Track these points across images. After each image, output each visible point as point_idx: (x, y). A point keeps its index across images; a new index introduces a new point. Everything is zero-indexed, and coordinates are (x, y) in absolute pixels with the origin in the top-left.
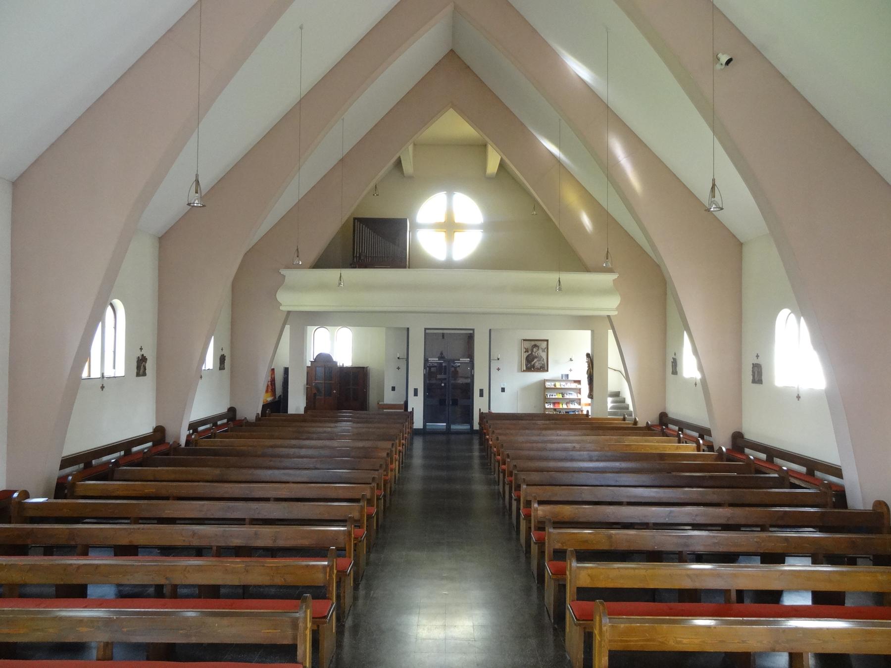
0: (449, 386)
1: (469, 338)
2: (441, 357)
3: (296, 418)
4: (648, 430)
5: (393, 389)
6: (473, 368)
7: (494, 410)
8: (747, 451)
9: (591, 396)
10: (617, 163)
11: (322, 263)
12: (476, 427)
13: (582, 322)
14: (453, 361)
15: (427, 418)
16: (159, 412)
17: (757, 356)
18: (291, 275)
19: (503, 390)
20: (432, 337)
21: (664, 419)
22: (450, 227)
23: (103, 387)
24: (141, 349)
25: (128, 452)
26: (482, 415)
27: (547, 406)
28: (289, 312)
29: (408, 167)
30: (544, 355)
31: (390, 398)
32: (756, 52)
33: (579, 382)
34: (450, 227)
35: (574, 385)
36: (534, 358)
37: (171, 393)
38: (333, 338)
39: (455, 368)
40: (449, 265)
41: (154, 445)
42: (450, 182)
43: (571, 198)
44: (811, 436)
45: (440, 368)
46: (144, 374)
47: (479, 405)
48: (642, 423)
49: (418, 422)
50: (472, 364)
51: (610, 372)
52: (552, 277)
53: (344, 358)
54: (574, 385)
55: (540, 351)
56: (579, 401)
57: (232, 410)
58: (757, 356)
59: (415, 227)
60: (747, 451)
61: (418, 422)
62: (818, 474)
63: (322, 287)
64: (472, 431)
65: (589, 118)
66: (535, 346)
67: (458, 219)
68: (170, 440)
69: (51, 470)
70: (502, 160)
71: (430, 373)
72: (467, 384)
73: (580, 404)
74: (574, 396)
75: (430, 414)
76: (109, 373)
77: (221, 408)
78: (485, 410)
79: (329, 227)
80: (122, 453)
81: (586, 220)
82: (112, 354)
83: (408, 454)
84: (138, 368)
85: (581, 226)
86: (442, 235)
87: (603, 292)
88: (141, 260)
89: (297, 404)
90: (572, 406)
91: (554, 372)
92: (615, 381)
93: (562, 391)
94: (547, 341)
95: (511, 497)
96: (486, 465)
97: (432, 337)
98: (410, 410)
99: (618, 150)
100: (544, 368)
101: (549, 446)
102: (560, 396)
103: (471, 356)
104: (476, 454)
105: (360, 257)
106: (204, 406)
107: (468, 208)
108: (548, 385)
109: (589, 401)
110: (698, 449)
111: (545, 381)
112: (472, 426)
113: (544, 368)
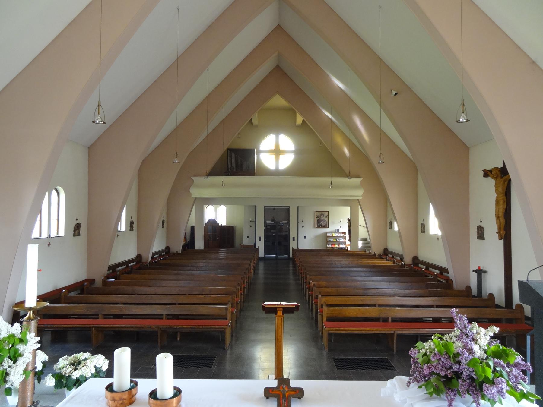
0: (277, 232)
1: (288, 210)
2: (273, 220)
3: (199, 251)
4: (380, 257)
5: (248, 237)
6: (289, 226)
7: (300, 248)
8: (420, 265)
9: (350, 240)
10: (357, 127)
11: (212, 174)
12: (291, 256)
13: (345, 202)
14: (279, 222)
15: (266, 251)
16: (138, 248)
17: (481, 221)
18: (198, 180)
19: (305, 237)
20: (267, 210)
21: (386, 252)
22: (277, 152)
23: (49, 244)
24: (77, 219)
25: (128, 266)
26: (293, 250)
27: (328, 246)
28: (196, 198)
29: (255, 122)
30: (326, 219)
31: (246, 242)
32: (408, 89)
33: (345, 233)
34: (277, 152)
35: (342, 235)
36: (321, 221)
37: (143, 239)
38: (216, 211)
39: (281, 226)
40: (277, 173)
41: (136, 264)
42: (278, 129)
43: (339, 139)
44: (436, 255)
45: (273, 227)
46: (133, 230)
47: (293, 245)
48: (377, 254)
49: (261, 254)
50: (289, 224)
51: (360, 227)
52: (328, 180)
53: (222, 221)
54: (342, 235)
55: (325, 217)
56: (345, 243)
57: (168, 248)
58: (481, 221)
59: (259, 152)
60: (420, 265)
61: (261, 254)
62: (444, 273)
63: (212, 186)
64: (289, 258)
65: (345, 105)
66: (322, 214)
67: (281, 148)
68: (144, 260)
69: (105, 271)
70: (303, 120)
71: (268, 229)
72: (287, 235)
73: (345, 244)
74: (342, 241)
75: (267, 250)
76: (54, 234)
77: (163, 247)
78: (296, 248)
79: (215, 155)
80: (125, 266)
81: (346, 151)
82: (56, 221)
83: (257, 269)
84: (130, 226)
85: (344, 153)
86: (273, 156)
87: (355, 187)
88: (73, 161)
89: (199, 244)
90: (341, 246)
91: (332, 228)
92: (362, 232)
93: (336, 238)
94: (328, 212)
95: (317, 312)
96: (295, 273)
97: (267, 210)
98: (257, 247)
99: (358, 121)
100: (327, 226)
101: (326, 262)
102: (335, 241)
103: (288, 220)
104: (291, 268)
105: (429, 362)
106: (157, 246)
107: (287, 142)
108: (329, 235)
109: (349, 243)
110: (394, 263)
111: (327, 233)
112: (289, 256)
113: (327, 226)
